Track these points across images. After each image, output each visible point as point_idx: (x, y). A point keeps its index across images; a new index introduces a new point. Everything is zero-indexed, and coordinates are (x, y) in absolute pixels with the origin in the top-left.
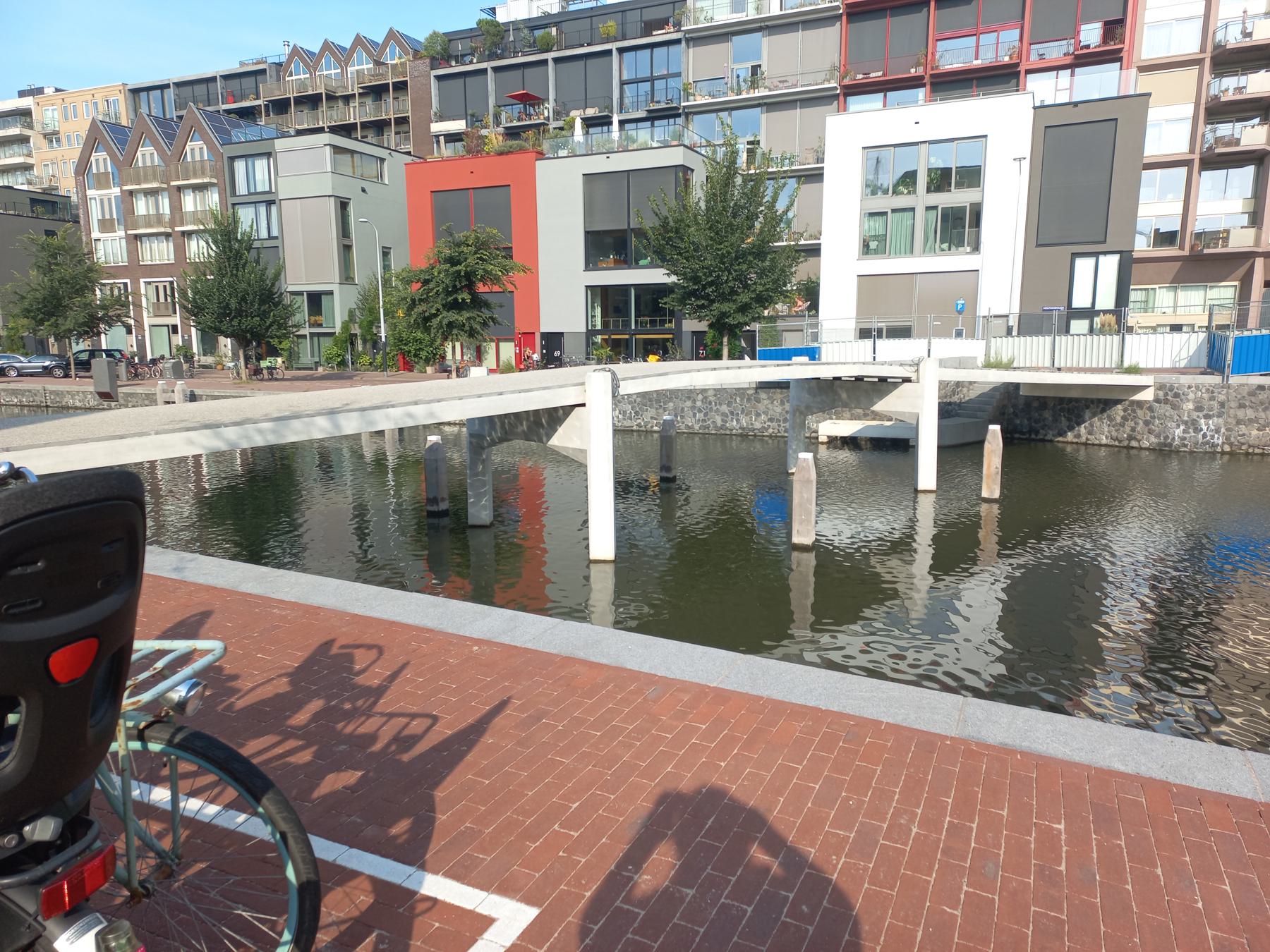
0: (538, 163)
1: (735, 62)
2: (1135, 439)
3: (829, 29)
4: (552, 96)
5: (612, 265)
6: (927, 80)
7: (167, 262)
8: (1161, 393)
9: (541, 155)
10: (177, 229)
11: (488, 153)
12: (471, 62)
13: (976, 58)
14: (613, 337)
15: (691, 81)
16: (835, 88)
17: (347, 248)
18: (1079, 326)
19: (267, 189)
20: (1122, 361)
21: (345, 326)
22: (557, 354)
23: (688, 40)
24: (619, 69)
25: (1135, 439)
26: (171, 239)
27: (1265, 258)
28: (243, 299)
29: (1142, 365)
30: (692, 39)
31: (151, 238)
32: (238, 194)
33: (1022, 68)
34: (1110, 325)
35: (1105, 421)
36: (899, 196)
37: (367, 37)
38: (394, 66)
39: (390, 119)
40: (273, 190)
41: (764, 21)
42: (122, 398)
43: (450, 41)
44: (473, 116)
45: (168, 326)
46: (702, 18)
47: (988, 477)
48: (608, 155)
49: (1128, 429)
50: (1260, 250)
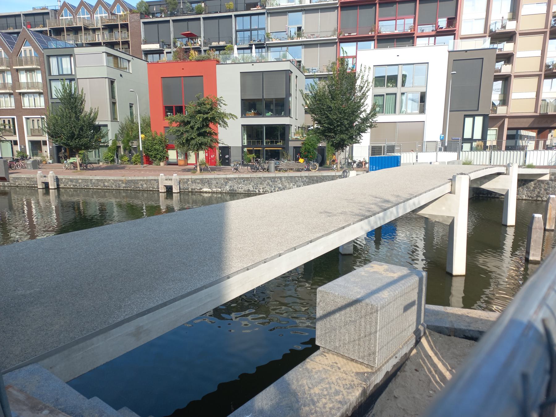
0: (217, 66)
1: (289, 25)
2: (540, 196)
3: (332, 13)
4: (202, 35)
5: (253, 115)
6: (375, 38)
7: (10, 108)
8: (553, 177)
9: (218, 62)
10: (17, 91)
11: (191, 60)
12: (161, 17)
13: (396, 30)
14: (255, 149)
15: (269, 32)
16: (336, 39)
17: (114, 104)
18: (467, 146)
19: (70, 73)
20: (525, 163)
21: (114, 142)
22: (227, 156)
23: (268, 13)
24: (237, 24)
25: (540, 196)
26: (12, 96)
27: (509, 118)
28: (81, 129)
29: (534, 164)
30: (270, 13)
31: (30, 95)
32: (52, 74)
33: (415, 35)
34: (481, 146)
35: (525, 189)
36: (389, 88)
37: (69, 4)
38: (120, 16)
39: (119, 42)
40: (73, 73)
41: (304, 7)
42: (12, 180)
43: (149, 6)
44: (163, 42)
45: (11, 141)
46: (275, 4)
47: (550, 219)
48: (253, 64)
49: (536, 193)
50: (507, 115)
